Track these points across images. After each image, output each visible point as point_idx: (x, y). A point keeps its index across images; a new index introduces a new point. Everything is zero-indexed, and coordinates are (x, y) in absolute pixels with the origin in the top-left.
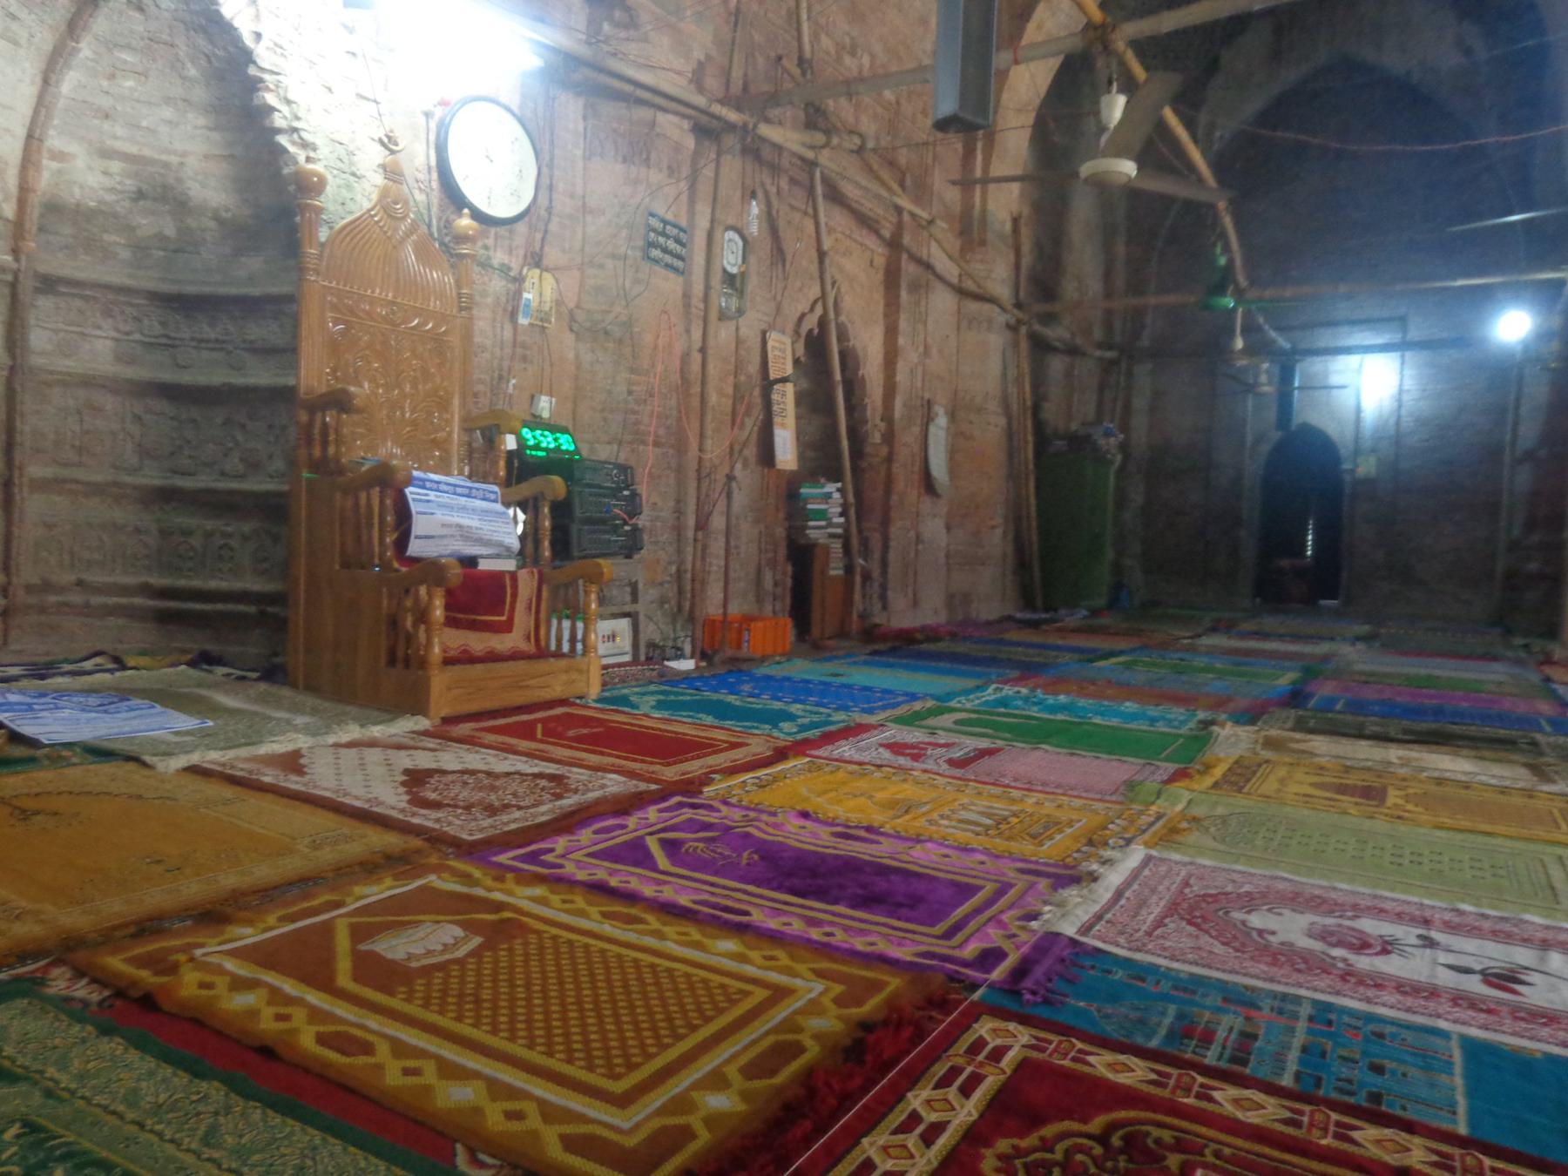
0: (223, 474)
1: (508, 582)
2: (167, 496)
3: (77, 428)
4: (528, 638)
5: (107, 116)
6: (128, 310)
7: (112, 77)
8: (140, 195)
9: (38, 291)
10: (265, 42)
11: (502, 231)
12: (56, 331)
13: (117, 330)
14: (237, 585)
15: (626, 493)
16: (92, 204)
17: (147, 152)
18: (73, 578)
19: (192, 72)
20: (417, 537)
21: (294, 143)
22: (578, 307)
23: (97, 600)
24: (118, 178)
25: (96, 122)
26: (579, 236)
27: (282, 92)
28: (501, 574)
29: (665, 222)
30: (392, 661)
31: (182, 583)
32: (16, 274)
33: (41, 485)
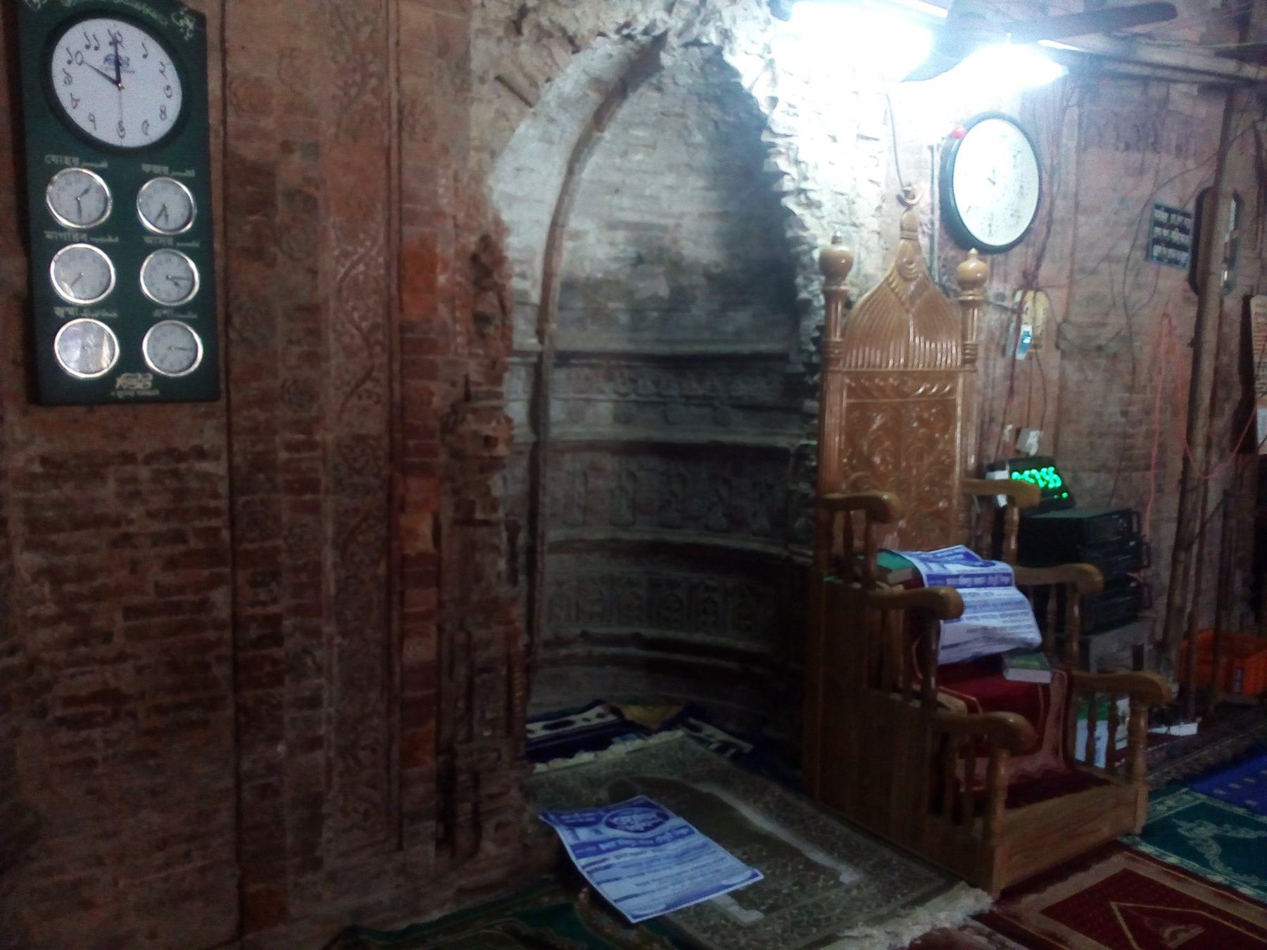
0: (707, 528)
1: (1041, 694)
2: (655, 550)
3: (582, 489)
4: (1056, 752)
5: (617, 191)
6: (627, 373)
7: (624, 154)
8: (639, 260)
9: (557, 366)
10: (781, 105)
11: (1000, 258)
12: (567, 400)
13: (616, 392)
14: (722, 641)
15: (1132, 543)
16: (600, 275)
17: (648, 218)
18: (577, 631)
19: (698, 138)
20: (944, 648)
21: (799, 204)
22: (1065, 320)
23: (598, 650)
24: (621, 247)
25: (608, 198)
26: (1070, 238)
27: (792, 154)
28: (1033, 686)
29: (1169, 211)
30: (936, 807)
31: (670, 634)
32: (540, 355)
33: (558, 547)
